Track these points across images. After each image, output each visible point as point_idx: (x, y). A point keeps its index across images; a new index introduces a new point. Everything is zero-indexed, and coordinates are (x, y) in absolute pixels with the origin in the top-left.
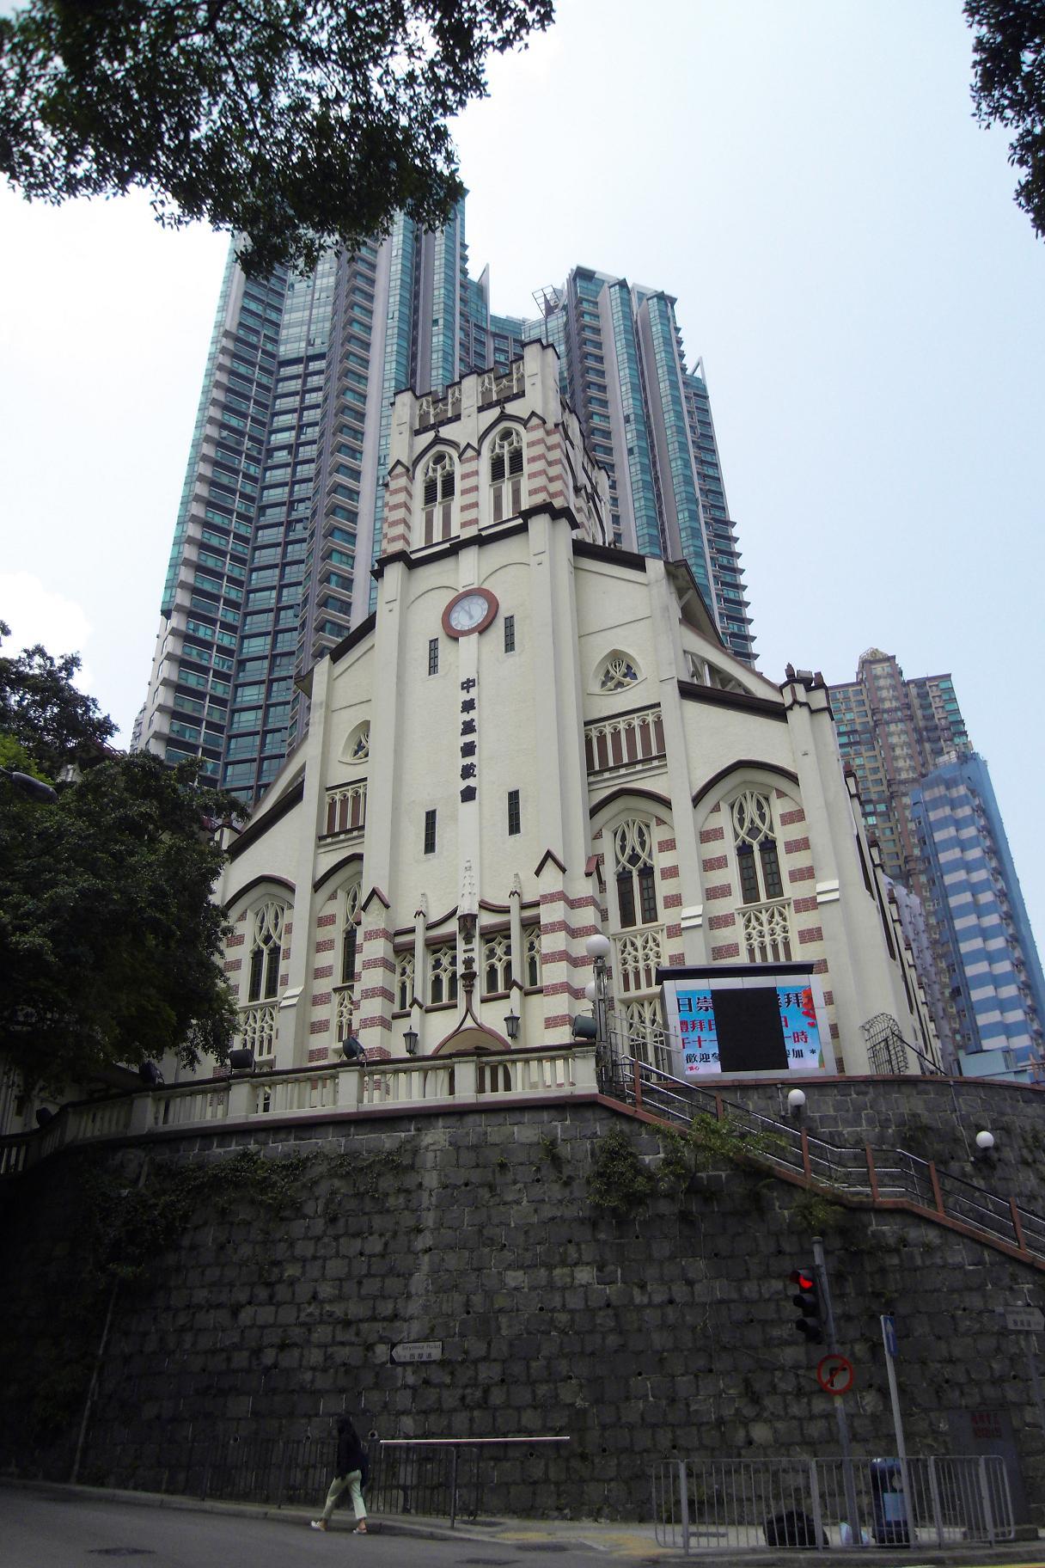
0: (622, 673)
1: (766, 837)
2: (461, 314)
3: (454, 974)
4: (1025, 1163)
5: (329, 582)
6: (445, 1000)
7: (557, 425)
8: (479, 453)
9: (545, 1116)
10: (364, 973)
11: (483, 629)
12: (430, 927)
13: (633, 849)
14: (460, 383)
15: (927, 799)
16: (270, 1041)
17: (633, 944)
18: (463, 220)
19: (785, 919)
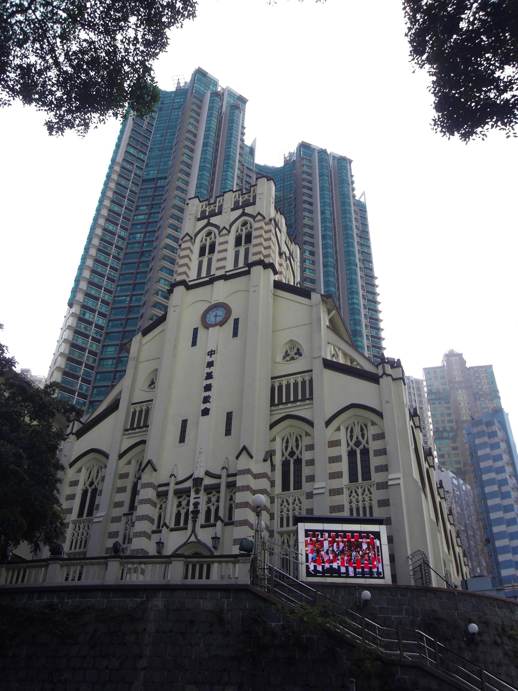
0: (294, 352)
1: (364, 447)
2: (239, 161)
3: (188, 510)
4: (496, 643)
5: (157, 295)
6: (182, 524)
7: (271, 220)
8: (229, 232)
9: (219, 595)
10: (139, 506)
11: (222, 324)
12: (178, 483)
13: (292, 448)
14: (223, 195)
15: (475, 432)
16: (86, 541)
17: (287, 501)
18: (244, 114)
19: (371, 493)
